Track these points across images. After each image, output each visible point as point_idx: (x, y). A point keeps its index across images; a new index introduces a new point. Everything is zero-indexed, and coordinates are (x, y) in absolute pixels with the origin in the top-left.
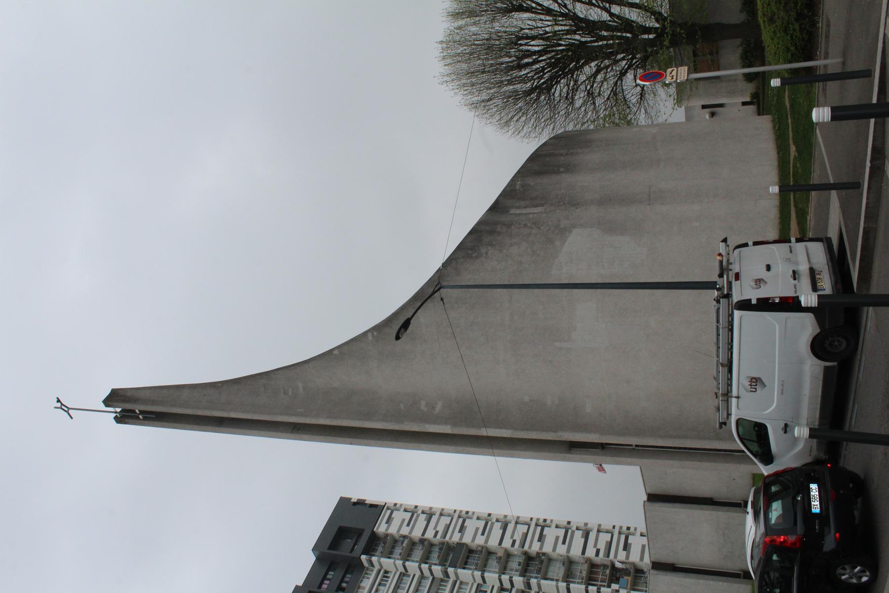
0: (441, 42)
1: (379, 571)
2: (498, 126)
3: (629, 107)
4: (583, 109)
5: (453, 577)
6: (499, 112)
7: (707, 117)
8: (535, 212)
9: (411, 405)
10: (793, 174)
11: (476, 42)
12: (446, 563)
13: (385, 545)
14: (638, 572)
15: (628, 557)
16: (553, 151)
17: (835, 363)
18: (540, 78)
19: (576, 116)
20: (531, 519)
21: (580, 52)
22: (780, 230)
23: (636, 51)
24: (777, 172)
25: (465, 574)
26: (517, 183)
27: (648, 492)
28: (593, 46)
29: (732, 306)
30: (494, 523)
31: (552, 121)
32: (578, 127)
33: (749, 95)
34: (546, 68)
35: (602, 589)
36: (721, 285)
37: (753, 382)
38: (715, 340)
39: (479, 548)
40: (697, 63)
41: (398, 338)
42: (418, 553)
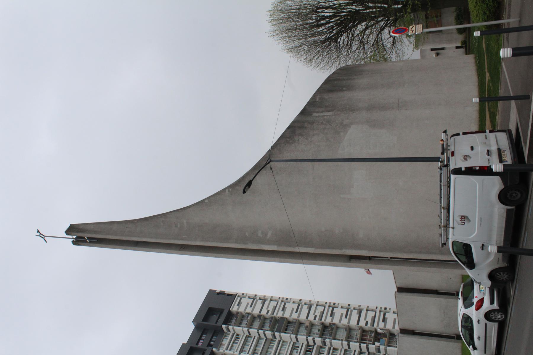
4: (357, 51)
5: (278, 338)
6: (306, 54)
7: (434, 56)
8: (328, 115)
10: (488, 91)
11: (291, 11)
12: (274, 330)
13: (237, 318)
14: (392, 335)
15: (385, 326)
16: (339, 78)
17: (513, 207)
18: (331, 33)
19: (353, 56)
20: (326, 303)
22: (479, 125)
23: (390, 15)
24: (478, 90)
25: (286, 336)
26: (317, 97)
27: (398, 286)
28: (364, 12)
32: (354, 63)
33: (460, 42)
34: (335, 27)
35: (370, 346)
37: (463, 219)
38: (439, 193)
39: (294, 321)
40: (428, 22)
41: (244, 192)
42: (257, 324)
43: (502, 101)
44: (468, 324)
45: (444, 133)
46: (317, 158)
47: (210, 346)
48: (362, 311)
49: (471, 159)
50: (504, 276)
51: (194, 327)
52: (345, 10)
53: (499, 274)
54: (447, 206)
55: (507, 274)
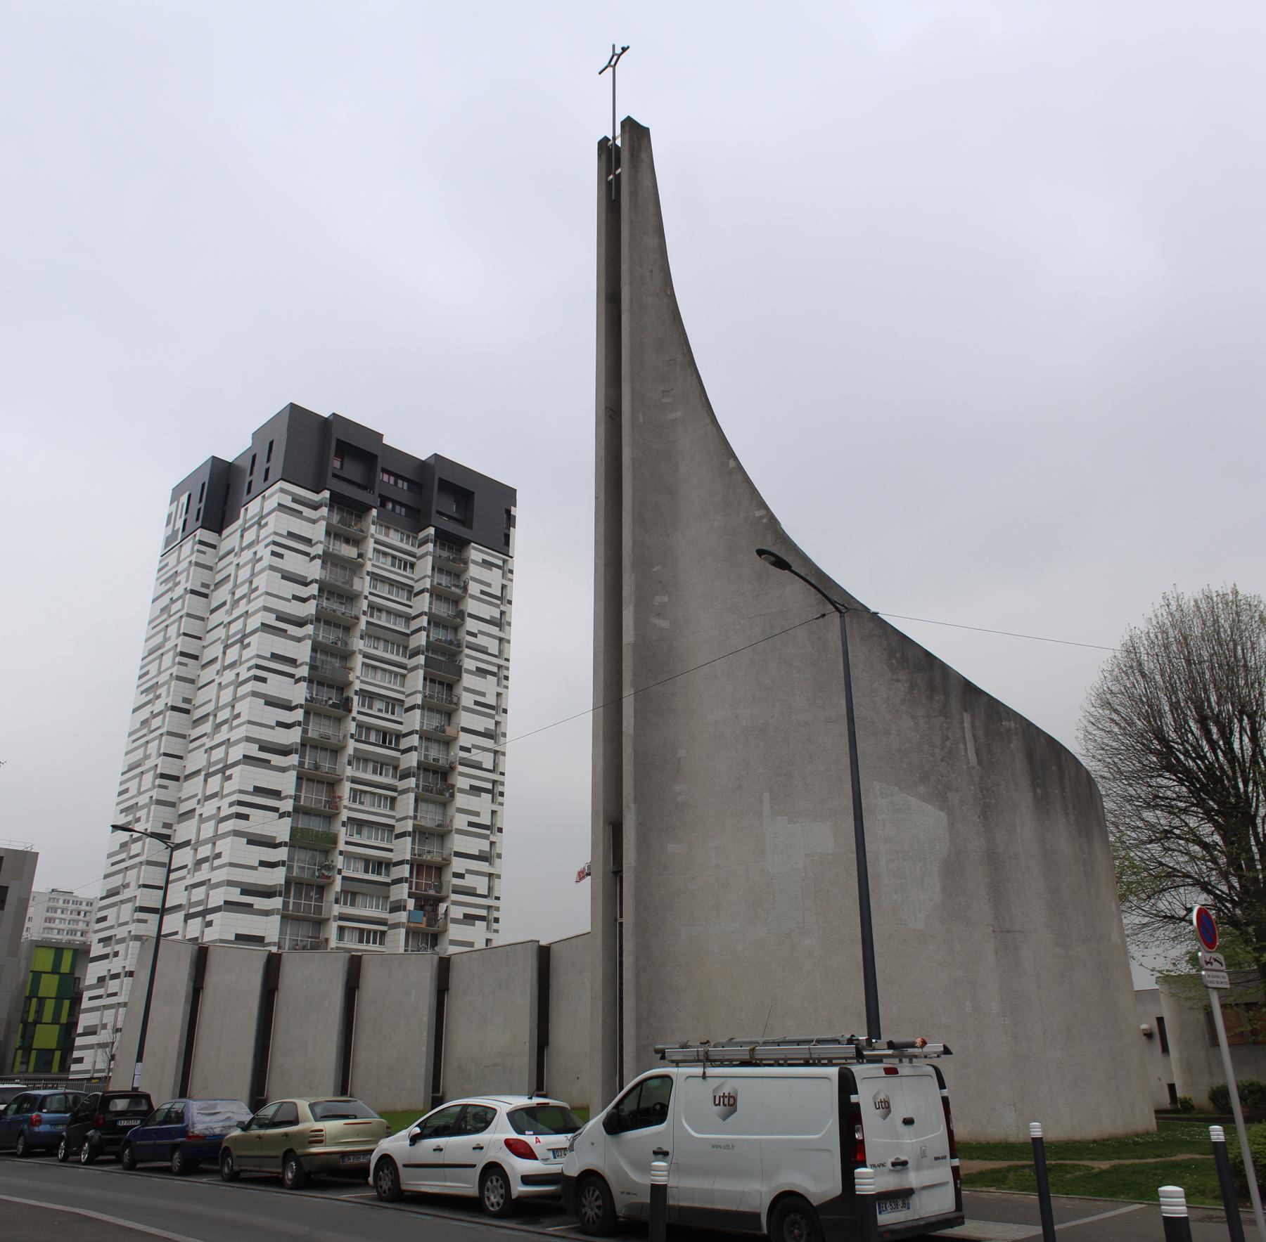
0: (1236, 593)
1: (414, 556)
2: (1101, 691)
3: (1149, 897)
4: (1140, 824)
5: (411, 663)
6: (1123, 691)
7: (1144, 1026)
8: (969, 752)
9: (660, 582)
10: (1062, 1165)
11: (1239, 648)
12: (430, 652)
14: (433, 938)
15: (455, 921)
16: (1067, 776)
17: (765, 1231)
18: (1186, 754)
20: (503, 774)
21: (1236, 817)
23: (1247, 908)
24: (1063, 1139)
25: (417, 680)
26: (1012, 722)
27: (553, 946)
28: (1249, 838)
29: (844, 1064)
30: (494, 718)
31: (1116, 776)
32: (1110, 817)
33: (1188, 1096)
34: (1203, 762)
35: (406, 885)
36: (876, 1045)
37: (729, 1100)
39: (455, 700)
40: (1235, 1008)
41: (760, 552)
42: (443, 610)
43: (1038, 1203)
44: (472, 1122)
45: (942, 1049)
46: (856, 730)
47: (381, 502)
48: (488, 864)
49: (882, 1120)
50: (591, 1208)
51: (423, 459)
52: (1253, 789)
53: (595, 1195)
54: (757, 1059)
55: (598, 1217)
